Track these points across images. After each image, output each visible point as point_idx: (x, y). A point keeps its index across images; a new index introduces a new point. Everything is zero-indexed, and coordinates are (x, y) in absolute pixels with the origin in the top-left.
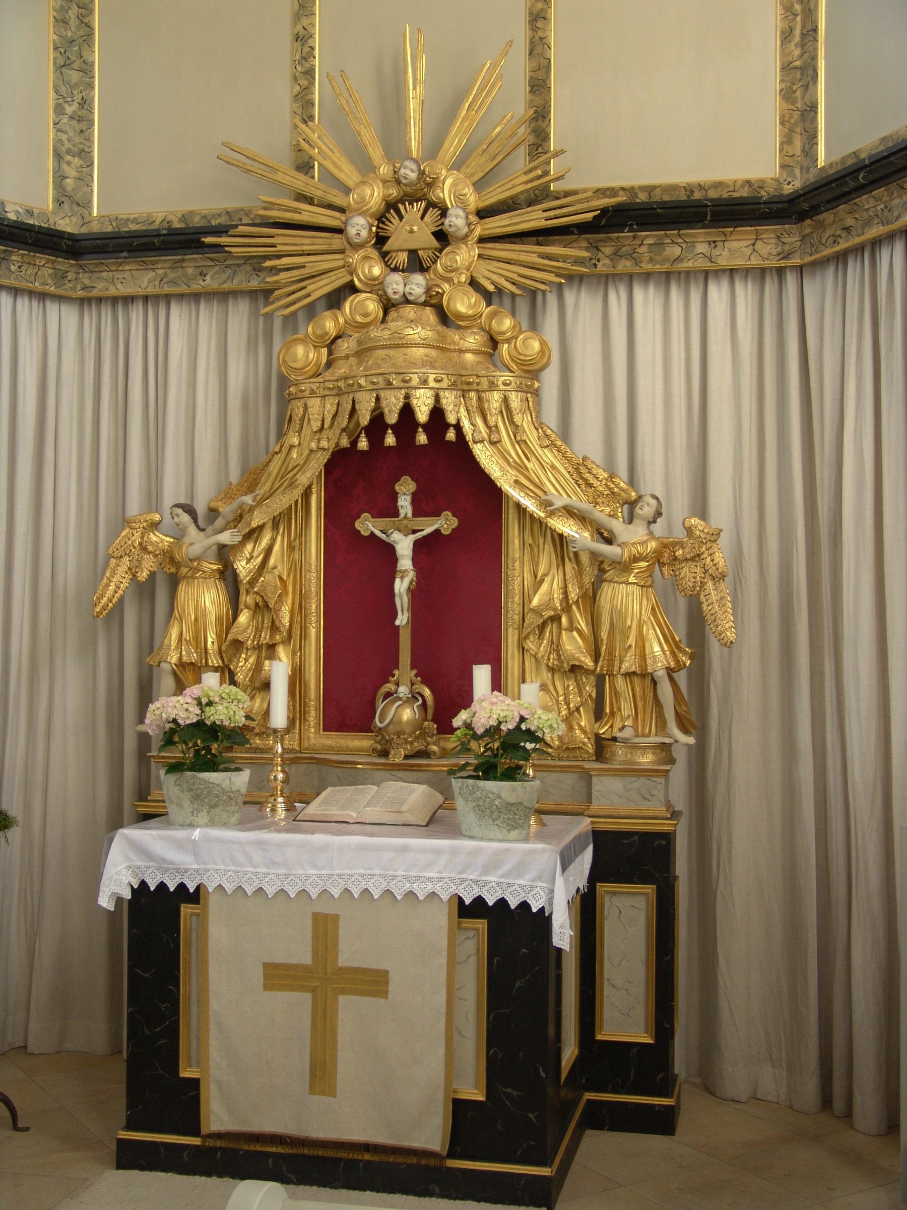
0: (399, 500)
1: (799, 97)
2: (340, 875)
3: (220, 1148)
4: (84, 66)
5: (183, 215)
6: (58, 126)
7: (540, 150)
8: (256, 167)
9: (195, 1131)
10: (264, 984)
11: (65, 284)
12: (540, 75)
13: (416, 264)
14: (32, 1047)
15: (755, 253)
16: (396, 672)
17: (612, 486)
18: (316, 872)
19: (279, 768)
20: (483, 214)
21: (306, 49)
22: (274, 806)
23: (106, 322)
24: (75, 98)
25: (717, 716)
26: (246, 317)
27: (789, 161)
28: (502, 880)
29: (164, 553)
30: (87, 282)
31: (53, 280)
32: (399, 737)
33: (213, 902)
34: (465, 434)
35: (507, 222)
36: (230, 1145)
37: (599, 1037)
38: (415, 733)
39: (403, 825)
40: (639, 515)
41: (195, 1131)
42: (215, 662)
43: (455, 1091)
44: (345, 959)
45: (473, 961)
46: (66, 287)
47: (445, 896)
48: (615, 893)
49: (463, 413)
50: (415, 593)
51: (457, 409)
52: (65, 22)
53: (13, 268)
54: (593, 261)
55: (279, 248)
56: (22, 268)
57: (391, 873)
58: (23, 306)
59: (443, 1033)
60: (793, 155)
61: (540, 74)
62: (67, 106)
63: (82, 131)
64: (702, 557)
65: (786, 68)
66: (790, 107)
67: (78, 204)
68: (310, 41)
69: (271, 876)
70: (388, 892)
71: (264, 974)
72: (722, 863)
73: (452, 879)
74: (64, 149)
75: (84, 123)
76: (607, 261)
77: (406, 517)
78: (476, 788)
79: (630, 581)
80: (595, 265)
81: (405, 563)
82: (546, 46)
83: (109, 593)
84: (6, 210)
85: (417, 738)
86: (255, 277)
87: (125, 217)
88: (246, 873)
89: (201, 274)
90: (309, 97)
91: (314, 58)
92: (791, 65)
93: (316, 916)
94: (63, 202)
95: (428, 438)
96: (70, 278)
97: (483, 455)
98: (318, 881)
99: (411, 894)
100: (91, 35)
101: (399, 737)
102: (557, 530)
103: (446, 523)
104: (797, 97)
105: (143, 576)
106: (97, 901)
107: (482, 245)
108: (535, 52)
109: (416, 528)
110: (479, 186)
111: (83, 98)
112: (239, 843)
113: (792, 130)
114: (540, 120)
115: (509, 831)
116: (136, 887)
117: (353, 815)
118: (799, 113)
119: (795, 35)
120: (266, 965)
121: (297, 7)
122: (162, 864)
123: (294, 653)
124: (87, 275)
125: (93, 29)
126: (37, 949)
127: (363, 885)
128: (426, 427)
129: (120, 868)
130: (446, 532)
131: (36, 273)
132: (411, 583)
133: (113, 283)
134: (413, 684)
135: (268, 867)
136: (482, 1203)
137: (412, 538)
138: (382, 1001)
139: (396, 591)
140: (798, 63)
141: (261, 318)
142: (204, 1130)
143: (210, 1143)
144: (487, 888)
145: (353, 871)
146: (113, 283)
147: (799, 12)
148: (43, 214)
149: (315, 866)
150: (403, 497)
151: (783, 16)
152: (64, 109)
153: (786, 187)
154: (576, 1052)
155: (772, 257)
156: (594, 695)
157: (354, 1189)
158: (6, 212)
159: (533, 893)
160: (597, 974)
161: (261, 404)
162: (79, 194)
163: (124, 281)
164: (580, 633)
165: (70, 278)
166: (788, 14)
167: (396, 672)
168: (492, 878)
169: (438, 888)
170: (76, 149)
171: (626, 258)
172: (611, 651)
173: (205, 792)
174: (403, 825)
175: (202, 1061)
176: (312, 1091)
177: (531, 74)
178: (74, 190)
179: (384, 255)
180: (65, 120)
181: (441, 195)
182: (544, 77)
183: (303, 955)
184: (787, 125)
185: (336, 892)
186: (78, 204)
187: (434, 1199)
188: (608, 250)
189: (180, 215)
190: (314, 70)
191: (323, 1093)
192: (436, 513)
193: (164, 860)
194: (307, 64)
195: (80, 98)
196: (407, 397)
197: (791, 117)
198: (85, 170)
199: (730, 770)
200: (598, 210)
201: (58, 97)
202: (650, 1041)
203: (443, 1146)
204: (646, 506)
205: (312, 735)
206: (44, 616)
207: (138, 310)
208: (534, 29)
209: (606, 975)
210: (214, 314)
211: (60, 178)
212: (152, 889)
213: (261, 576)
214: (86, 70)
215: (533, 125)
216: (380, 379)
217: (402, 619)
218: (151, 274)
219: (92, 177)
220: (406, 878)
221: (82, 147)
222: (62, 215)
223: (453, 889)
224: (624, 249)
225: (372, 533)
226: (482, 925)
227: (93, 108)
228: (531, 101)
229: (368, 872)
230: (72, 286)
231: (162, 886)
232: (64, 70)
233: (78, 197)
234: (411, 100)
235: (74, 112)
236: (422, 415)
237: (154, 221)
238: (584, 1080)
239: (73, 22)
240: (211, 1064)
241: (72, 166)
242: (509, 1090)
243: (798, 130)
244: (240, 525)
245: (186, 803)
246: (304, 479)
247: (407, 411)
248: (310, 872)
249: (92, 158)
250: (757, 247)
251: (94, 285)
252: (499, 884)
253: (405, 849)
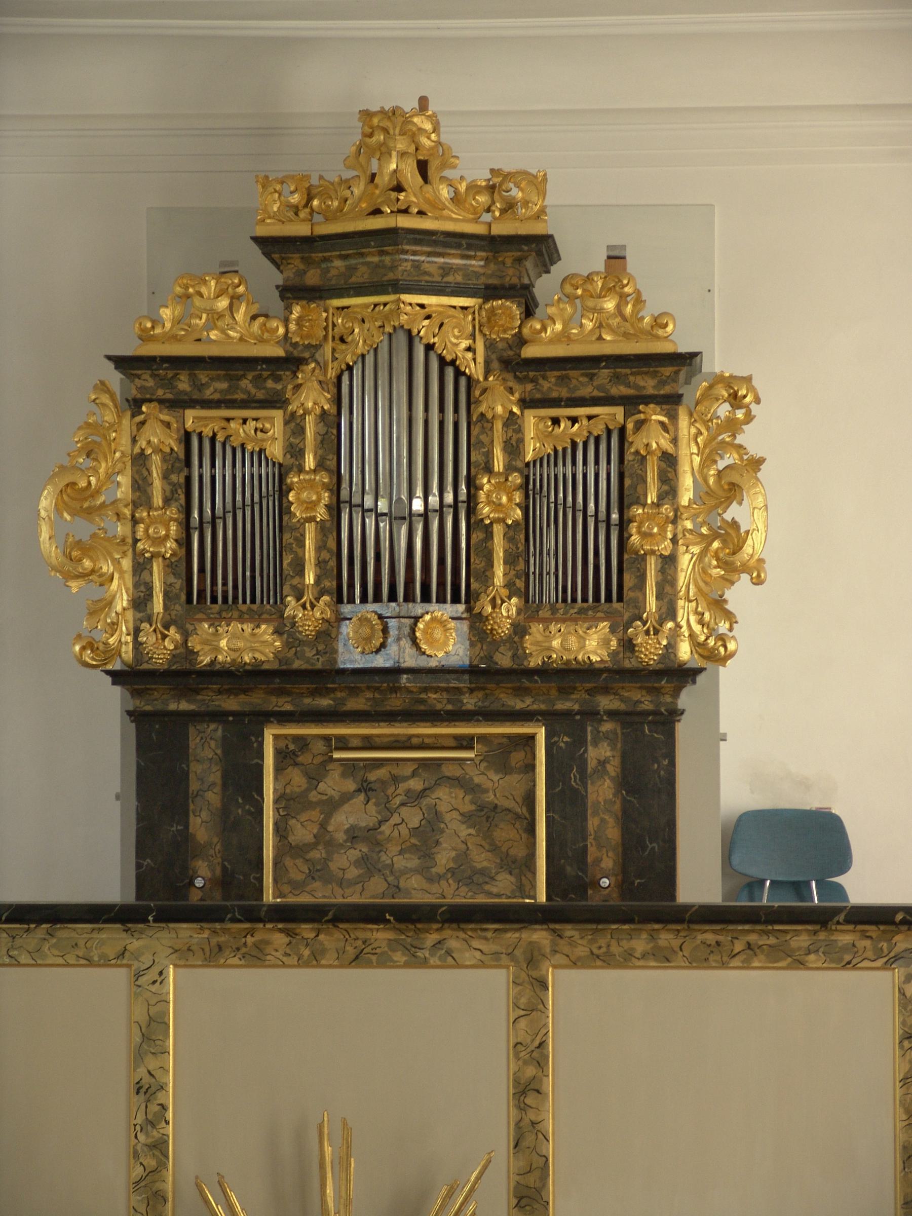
90: (159, 1186)
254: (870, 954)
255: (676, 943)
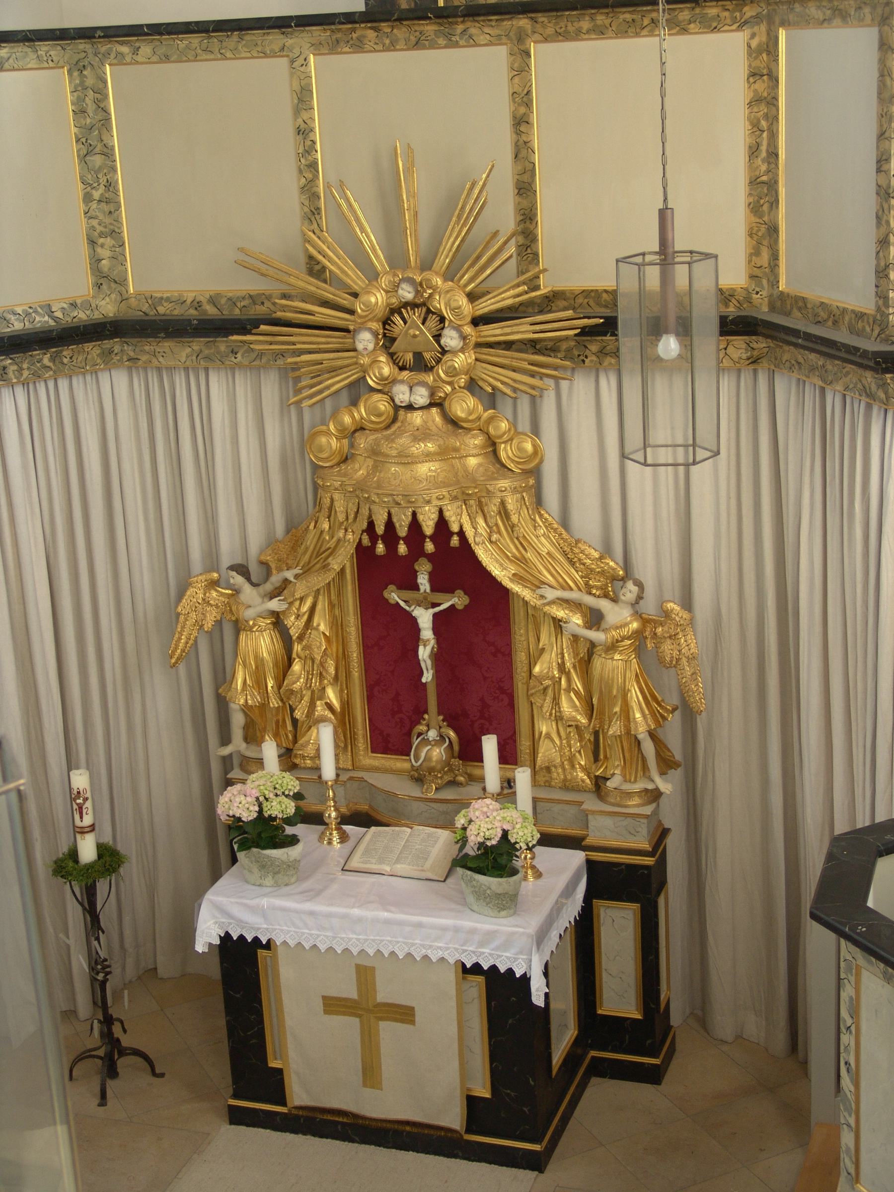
0: (419, 577)
1: (766, 211)
2: (373, 940)
3: (302, 1116)
4: (105, 150)
5: (211, 297)
6: (88, 215)
7: (529, 251)
8: (271, 272)
9: (283, 1103)
10: (324, 1010)
11: (112, 359)
12: (526, 177)
13: (421, 365)
14: (161, 972)
15: (727, 356)
16: (426, 716)
17: (603, 565)
18: (355, 936)
19: (332, 809)
20: (476, 322)
21: (308, 143)
22: (330, 839)
23: (153, 380)
24: (101, 181)
25: (703, 746)
26: (277, 386)
27: (757, 272)
28: (493, 952)
29: (225, 605)
30: (132, 354)
31: (101, 359)
32: (430, 774)
33: (281, 952)
34: (468, 537)
35: (498, 332)
36: (310, 1114)
37: (599, 1012)
38: (443, 770)
39: (426, 879)
40: (622, 600)
41: (283, 1103)
42: (275, 703)
43: (469, 1090)
44: (381, 997)
45: (476, 1001)
46: (113, 361)
47: (452, 961)
48: (609, 907)
49: (465, 520)
50: (437, 658)
51: (459, 517)
52: (83, 111)
53: (65, 361)
54: (582, 358)
55: (298, 346)
56: (74, 358)
57: (410, 941)
58: (78, 384)
59: (457, 1052)
60: (761, 267)
61: (526, 178)
62: (94, 192)
63: (110, 212)
64: (677, 637)
65: (754, 182)
66: (758, 220)
67: (116, 282)
68: (311, 134)
69: (322, 937)
70: (409, 955)
71: (324, 1004)
72: (709, 863)
73: (456, 949)
74: (96, 234)
75: (112, 205)
76: (594, 358)
77: (425, 591)
78: (472, 879)
79: (615, 658)
80: (583, 361)
81: (427, 633)
82: (530, 150)
83: (181, 645)
84: (53, 310)
85: (445, 773)
86: (281, 357)
87: (158, 295)
88: (303, 933)
89: (232, 352)
90: (315, 189)
91: (316, 151)
92: (758, 180)
93: (358, 967)
94: (101, 284)
95: (435, 547)
96: (116, 351)
97: (484, 555)
98: (358, 943)
99: (426, 957)
100: (108, 119)
101: (430, 774)
102: (552, 614)
103: (458, 600)
104: (763, 211)
105: (209, 625)
106: (194, 947)
107: (478, 350)
108: (520, 156)
109: (435, 601)
110: (472, 297)
111: (108, 181)
112: (296, 912)
113: (759, 243)
114: (528, 222)
115: (499, 911)
116: (222, 935)
117: (387, 868)
118: (766, 227)
119: (761, 151)
120: (324, 998)
121: (296, 101)
122: (240, 922)
123: (341, 691)
124: (130, 348)
125: (109, 114)
126: (156, 902)
127: (391, 948)
128: (433, 538)
129: (209, 924)
130: (460, 607)
131: (86, 358)
132: (433, 648)
133: (155, 356)
134: (440, 727)
135: (319, 930)
136: (493, 1165)
137: (432, 611)
138: (412, 1026)
139: (420, 657)
140: (764, 178)
141: (290, 379)
142: (290, 1104)
143: (294, 1112)
144: (482, 956)
145: (384, 938)
146: (155, 356)
147: (766, 128)
148: (87, 305)
149: (354, 932)
150: (422, 576)
151: (750, 132)
152: (92, 195)
153: (754, 296)
154: (576, 1032)
155: (742, 361)
156: (592, 739)
157: (401, 1149)
158: (53, 312)
159: (517, 963)
160: (596, 962)
161: (297, 461)
162: (115, 273)
163: (164, 354)
164: (577, 694)
165: (116, 351)
166: (755, 129)
167: (426, 716)
168: (486, 950)
169: (446, 956)
170: (107, 230)
171: (611, 356)
172: (602, 713)
173: (269, 863)
174: (426, 879)
175: (282, 1054)
176: (365, 1085)
177: (517, 177)
178: (110, 269)
179: (391, 355)
180: (94, 205)
181: (438, 305)
182: (530, 181)
183: (352, 993)
184: (755, 237)
185: (371, 952)
186: (116, 282)
187: (458, 1160)
188: (594, 348)
189: (208, 297)
190: (317, 163)
191: (373, 1087)
192: (451, 591)
193: (242, 921)
194: (310, 158)
195: (105, 180)
196: (414, 514)
197: (758, 231)
198: (117, 249)
199: (714, 791)
200: (578, 328)
201: (85, 187)
202: (639, 1017)
203: (462, 1126)
204: (628, 592)
205: (361, 757)
206: (130, 640)
207: (180, 374)
208: (518, 132)
209: (604, 967)
210: (249, 378)
211: (96, 261)
212: (235, 939)
213: (308, 630)
214: (108, 152)
215: (522, 226)
216: (390, 499)
217: (427, 677)
218: (189, 350)
219: (125, 257)
220: (423, 946)
221: (112, 227)
222: (102, 296)
223: (457, 956)
224: (608, 348)
225: (398, 603)
226: (481, 979)
227: (118, 191)
228: (519, 203)
229: (394, 939)
230: (118, 358)
231: (242, 938)
232: (88, 158)
233: (114, 275)
234: (406, 211)
235: (102, 194)
236: (428, 528)
237: (185, 301)
238: (590, 1041)
239: (91, 108)
240: (290, 1061)
241: (106, 247)
242: (509, 1091)
243: (765, 243)
244: (285, 591)
245: (256, 870)
246: (335, 565)
247: (415, 525)
248: (351, 936)
249: (123, 238)
250: (729, 351)
251: (139, 357)
252: (491, 955)
253: (420, 925)
254: (728, 21)
255: (607, 22)
